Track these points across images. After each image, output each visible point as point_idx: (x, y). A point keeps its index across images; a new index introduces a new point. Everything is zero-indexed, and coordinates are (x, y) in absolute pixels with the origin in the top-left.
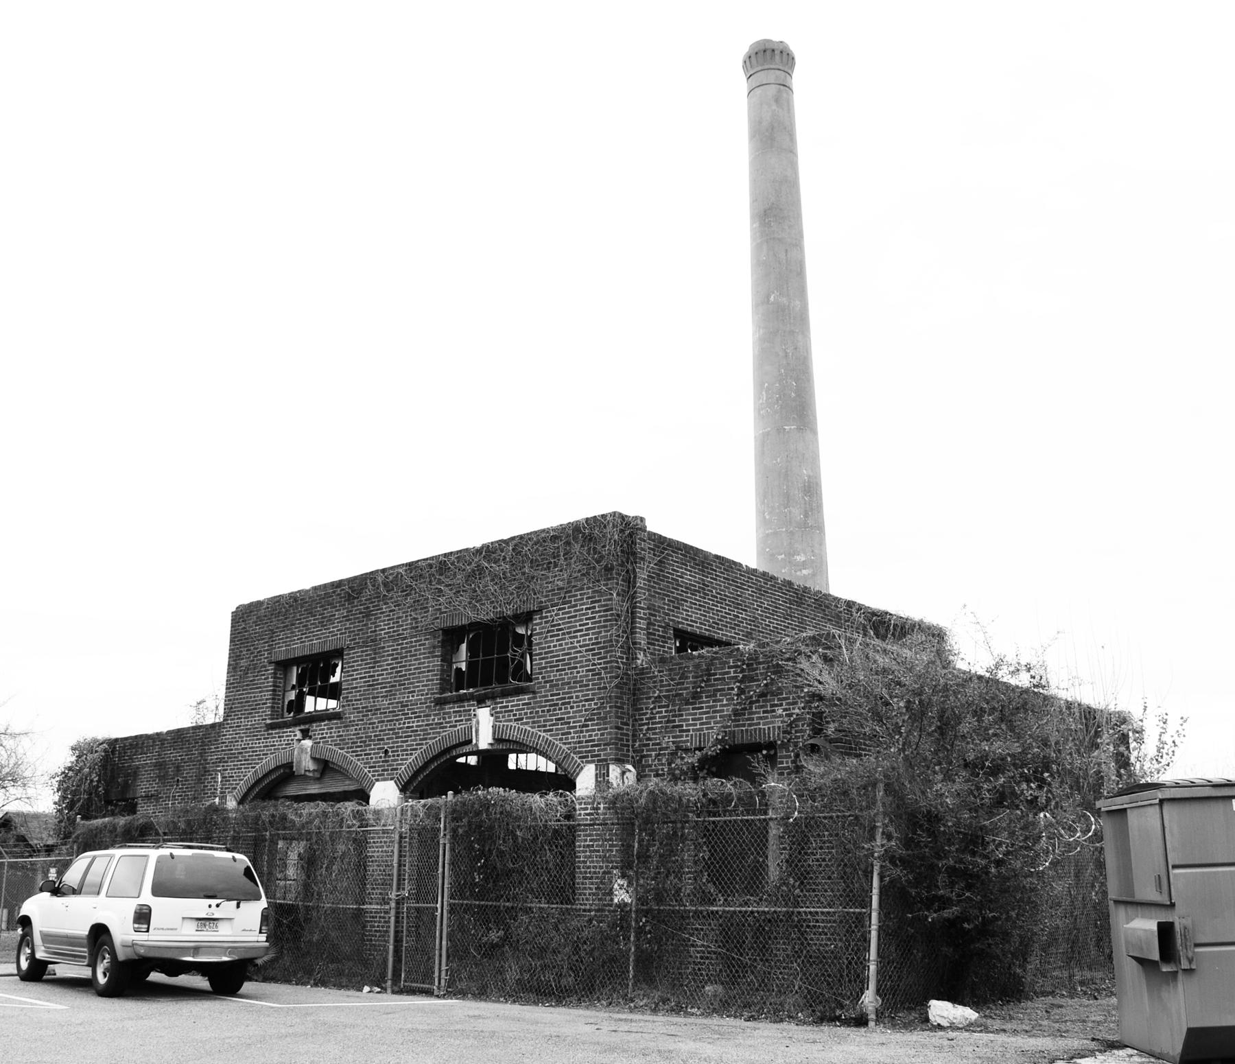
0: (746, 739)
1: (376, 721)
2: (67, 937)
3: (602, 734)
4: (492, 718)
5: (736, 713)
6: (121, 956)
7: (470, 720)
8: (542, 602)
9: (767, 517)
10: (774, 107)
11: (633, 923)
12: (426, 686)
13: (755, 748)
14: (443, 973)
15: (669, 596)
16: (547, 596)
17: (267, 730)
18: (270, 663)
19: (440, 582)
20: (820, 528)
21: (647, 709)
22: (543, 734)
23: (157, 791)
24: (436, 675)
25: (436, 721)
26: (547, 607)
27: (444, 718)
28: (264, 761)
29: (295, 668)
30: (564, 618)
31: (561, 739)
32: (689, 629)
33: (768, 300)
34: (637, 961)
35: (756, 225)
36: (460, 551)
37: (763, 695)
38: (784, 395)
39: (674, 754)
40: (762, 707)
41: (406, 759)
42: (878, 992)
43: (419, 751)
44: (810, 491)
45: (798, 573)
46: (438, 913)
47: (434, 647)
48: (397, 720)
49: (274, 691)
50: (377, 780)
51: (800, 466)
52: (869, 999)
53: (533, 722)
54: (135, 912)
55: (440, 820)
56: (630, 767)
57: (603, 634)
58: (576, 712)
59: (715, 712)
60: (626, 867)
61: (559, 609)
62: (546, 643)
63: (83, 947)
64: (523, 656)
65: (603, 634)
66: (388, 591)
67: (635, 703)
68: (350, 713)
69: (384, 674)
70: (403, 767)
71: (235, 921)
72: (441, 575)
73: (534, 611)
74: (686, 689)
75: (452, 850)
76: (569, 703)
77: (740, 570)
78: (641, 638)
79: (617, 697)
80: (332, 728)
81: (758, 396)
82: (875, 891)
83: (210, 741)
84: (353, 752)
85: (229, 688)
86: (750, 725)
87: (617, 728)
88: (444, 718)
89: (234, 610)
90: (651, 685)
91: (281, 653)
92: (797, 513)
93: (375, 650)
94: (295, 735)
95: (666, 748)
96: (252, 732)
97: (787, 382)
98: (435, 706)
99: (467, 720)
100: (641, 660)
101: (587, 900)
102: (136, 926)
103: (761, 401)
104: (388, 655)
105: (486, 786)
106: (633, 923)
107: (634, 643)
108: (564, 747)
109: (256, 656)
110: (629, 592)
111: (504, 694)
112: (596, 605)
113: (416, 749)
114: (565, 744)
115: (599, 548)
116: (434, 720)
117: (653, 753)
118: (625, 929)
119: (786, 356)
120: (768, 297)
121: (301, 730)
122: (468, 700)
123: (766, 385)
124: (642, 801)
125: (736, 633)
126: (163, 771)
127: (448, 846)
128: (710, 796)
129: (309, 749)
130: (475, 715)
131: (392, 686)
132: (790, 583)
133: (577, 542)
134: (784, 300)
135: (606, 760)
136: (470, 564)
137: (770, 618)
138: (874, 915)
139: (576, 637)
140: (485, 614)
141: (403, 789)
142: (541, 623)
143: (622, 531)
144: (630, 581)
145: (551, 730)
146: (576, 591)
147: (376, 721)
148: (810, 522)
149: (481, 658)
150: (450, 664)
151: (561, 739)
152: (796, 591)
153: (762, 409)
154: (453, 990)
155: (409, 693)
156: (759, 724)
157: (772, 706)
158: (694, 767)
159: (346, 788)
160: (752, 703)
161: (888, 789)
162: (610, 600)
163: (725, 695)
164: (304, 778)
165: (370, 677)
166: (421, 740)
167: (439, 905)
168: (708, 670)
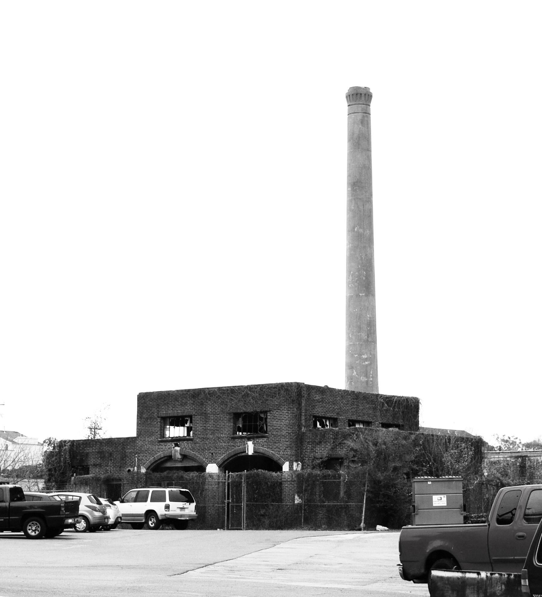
0: (335, 456)
1: (208, 443)
2: (133, 514)
3: (291, 453)
4: (253, 445)
5: (332, 448)
6: (160, 518)
7: (245, 445)
8: (270, 408)
9: (351, 336)
10: (360, 126)
11: (303, 508)
12: (228, 432)
13: (337, 459)
14: (245, 524)
15: (311, 405)
16: (272, 407)
17: (159, 443)
18: (158, 417)
19: (232, 396)
20: (374, 342)
21: (305, 445)
22: (271, 451)
23: (100, 463)
24: (231, 429)
25: (232, 444)
26: (272, 410)
27: (235, 444)
28: (158, 454)
29: (168, 420)
30: (278, 415)
31: (277, 453)
32: (318, 415)
33: (354, 230)
34: (304, 518)
35: (350, 189)
36: (239, 386)
37: (340, 444)
38: (360, 278)
39: (313, 459)
40: (340, 447)
41: (221, 457)
42: (364, 523)
43: (225, 454)
44: (370, 325)
45: (364, 363)
46: (243, 506)
47: (230, 419)
48: (216, 443)
49: (161, 428)
50: (209, 463)
51: (366, 313)
52: (362, 525)
53: (268, 447)
54: (165, 506)
55: (242, 479)
56: (299, 463)
57: (291, 421)
58: (283, 445)
59: (326, 447)
60: (299, 493)
61: (277, 411)
62: (272, 422)
63: (142, 517)
64: (263, 424)
65: (291, 421)
66: (210, 396)
67: (301, 443)
68: (196, 439)
69: (210, 425)
70: (219, 459)
71: (189, 509)
72: (232, 393)
73: (267, 411)
74: (317, 440)
75: (247, 488)
76: (280, 442)
77: (335, 391)
78: (303, 422)
79: (296, 441)
80: (189, 444)
81: (348, 278)
82: (365, 499)
83: (127, 444)
84: (198, 453)
85: (139, 425)
86: (336, 452)
87: (296, 451)
88: (235, 444)
89: (138, 394)
90: (306, 438)
91: (163, 413)
92: (364, 336)
93: (206, 417)
94: (172, 445)
95: (311, 457)
96: (152, 443)
97: (361, 272)
98: (231, 439)
99: (244, 445)
100: (303, 429)
101: (287, 503)
102: (166, 510)
103: (349, 280)
104: (212, 420)
105: (257, 469)
106: (303, 508)
107: (301, 424)
108: (278, 456)
109: (151, 414)
110: (299, 408)
111: (258, 437)
112: (289, 412)
113: (224, 453)
114: (279, 455)
115: (290, 394)
116: (231, 444)
117: (307, 459)
118: (301, 510)
119: (362, 259)
120: (354, 228)
121: (175, 444)
122: (244, 438)
123: (352, 272)
124: (306, 475)
125: (333, 414)
126: (102, 454)
127: (245, 487)
128: (324, 475)
129: (179, 451)
130: (247, 443)
131: (214, 431)
132: (354, 392)
133: (282, 390)
134: (361, 231)
135: (292, 461)
136: (243, 391)
137: (345, 406)
138: (364, 505)
139: (282, 421)
140: (250, 409)
141: (219, 467)
142: (270, 415)
143: (297, 389)
144: (300, 404)
145: (274, 450)
146: (282, 406)
147: (208, 443)
148: (370, 339)
149: (247, 424)
150: (236, 425)
151: (277, 453)
152: (356, 395)
153: (350, 284)
154: (248, 528)
155: (221, 434)
156: (338, 452)
157: (343, 447)
158: (319, 464)
159: (193, 465)
160: (337, 446)
161: (369, 474)
162: (294, 411)
163: (329, 443)
164: (176, 461)
165: (204, 427)
166: (226, 450)
167: (243, 504)
168: (324, 435)
